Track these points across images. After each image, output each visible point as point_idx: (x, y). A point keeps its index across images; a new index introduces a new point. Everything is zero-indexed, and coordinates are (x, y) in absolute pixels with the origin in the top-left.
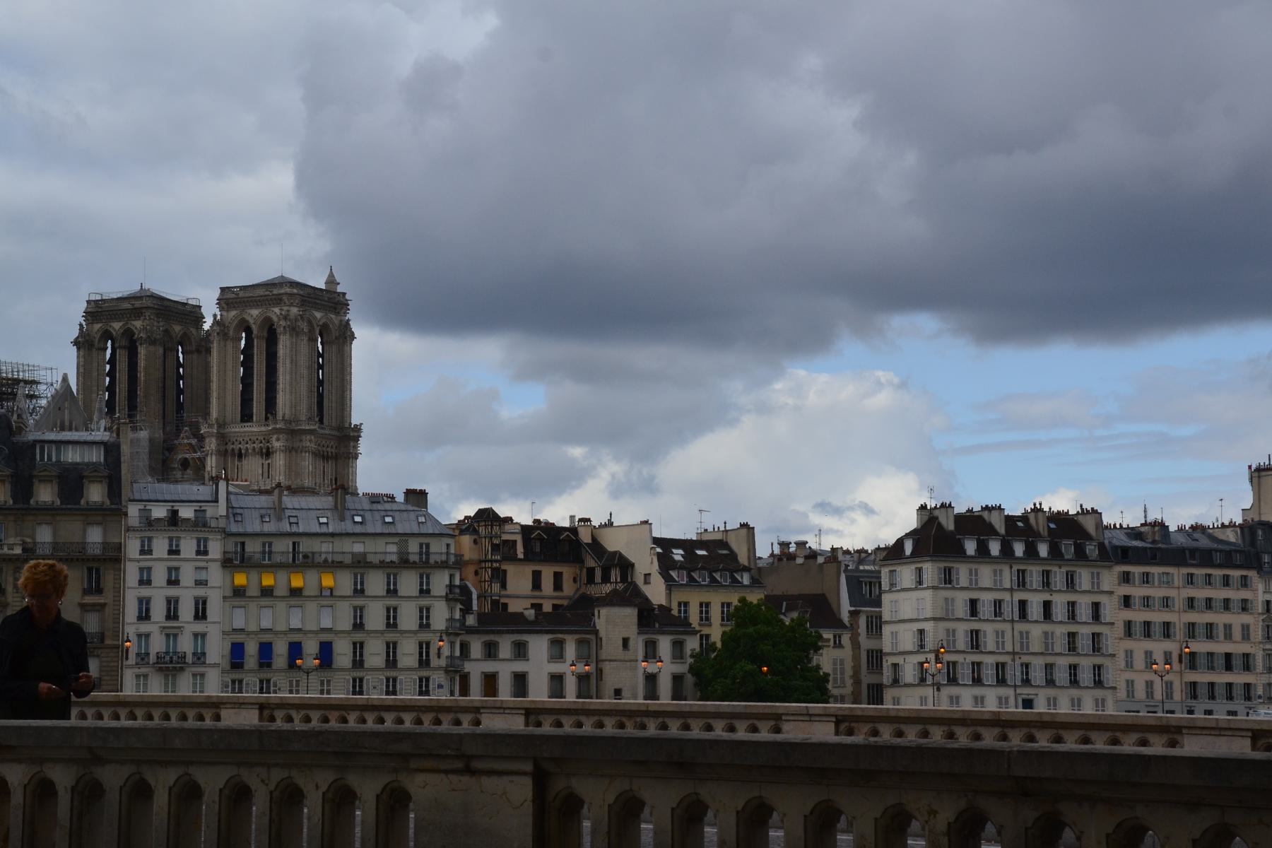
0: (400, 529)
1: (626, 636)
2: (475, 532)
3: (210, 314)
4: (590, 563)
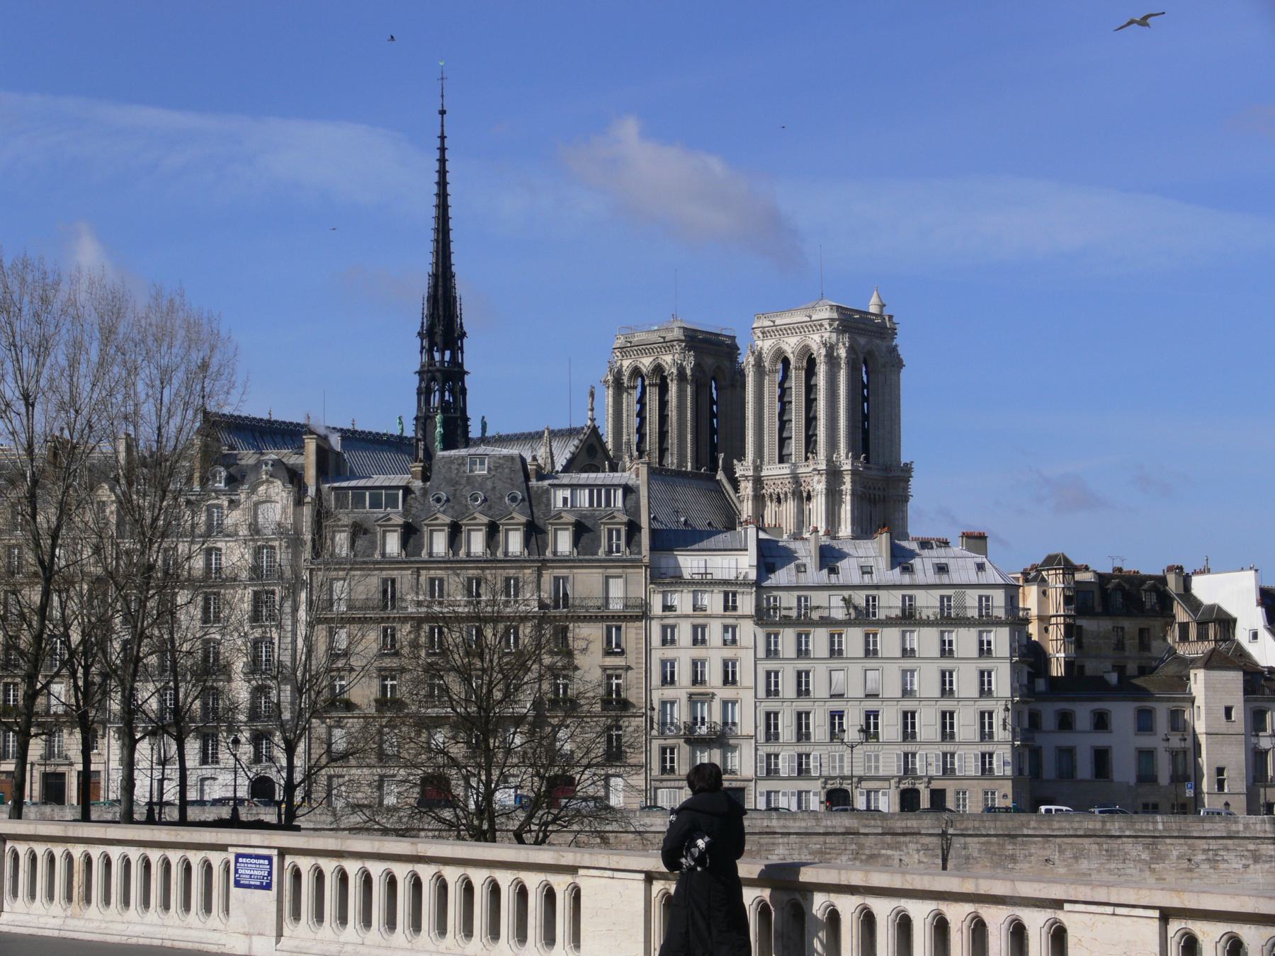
1: (1229, 704)
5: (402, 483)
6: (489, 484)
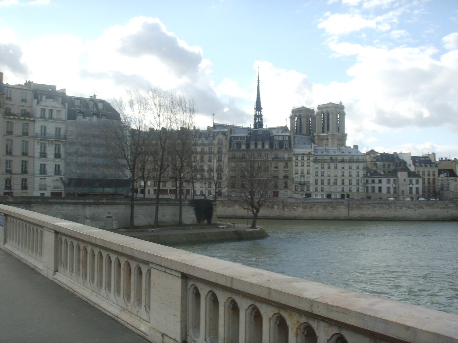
2: (370, 155)
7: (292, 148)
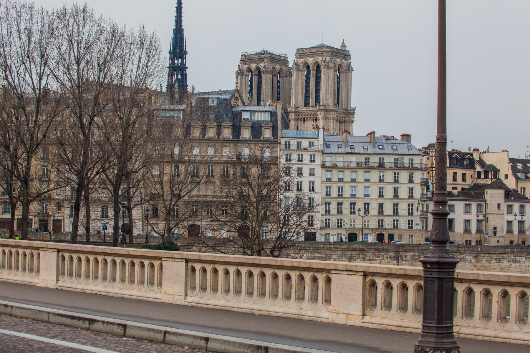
0: (400, 152)
1: (499, 203)
2: (428, 154)
3: (292, 60)
4: (479, 168)
5: (246, 107)
6: (217, 110)
7: (279, 138)
